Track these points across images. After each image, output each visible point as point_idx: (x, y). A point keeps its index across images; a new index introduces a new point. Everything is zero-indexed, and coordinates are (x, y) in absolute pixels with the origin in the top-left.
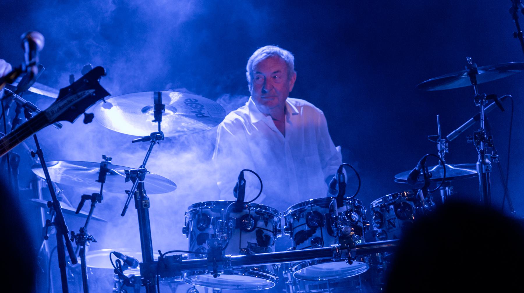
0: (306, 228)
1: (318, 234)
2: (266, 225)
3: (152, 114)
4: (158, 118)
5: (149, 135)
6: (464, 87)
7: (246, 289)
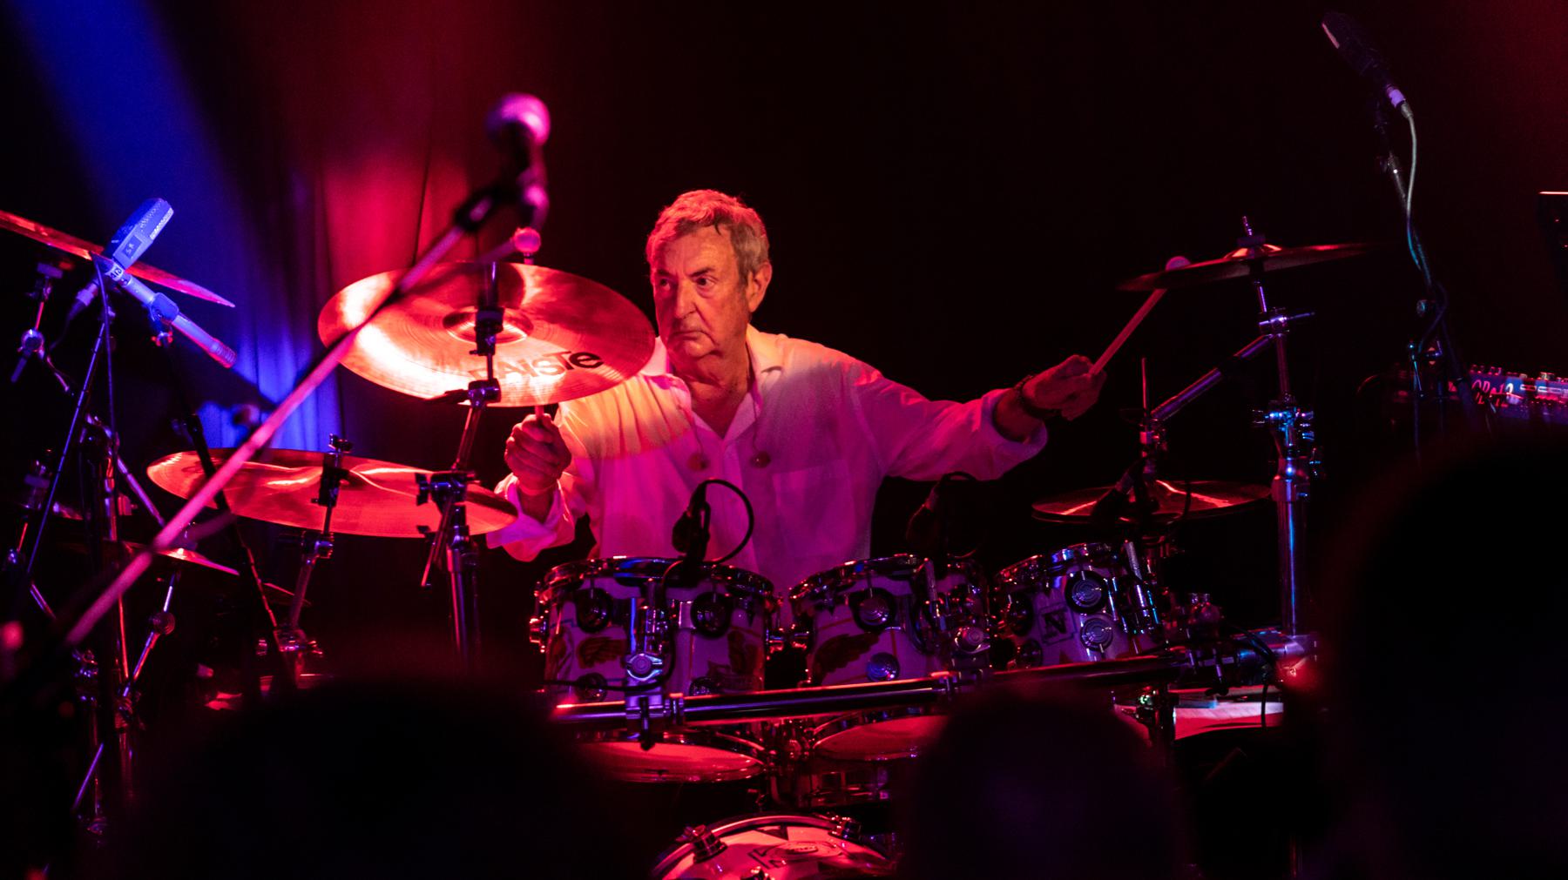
0: (854, 631)
1: (883, 645)
2: (751, 620)
3: (466, 336)
4: (485, 342)
5: (466, 388)
6: (256, 521)
7: (660, 772)
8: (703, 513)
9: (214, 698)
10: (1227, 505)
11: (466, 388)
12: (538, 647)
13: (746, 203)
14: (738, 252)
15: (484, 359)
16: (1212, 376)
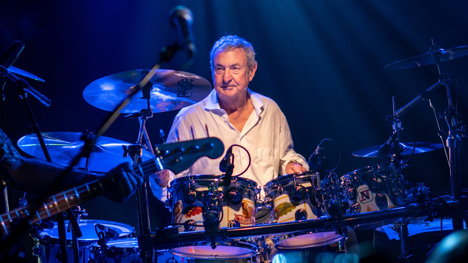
5: (139, 112)
8: (231, 158)
9: (43, 231)
10: (423, 151)
11: (139, 112)
12: (168, 209)
13: (247, 40)
14: (247, 56)
15: (146, 100)
16: (6, 191)
